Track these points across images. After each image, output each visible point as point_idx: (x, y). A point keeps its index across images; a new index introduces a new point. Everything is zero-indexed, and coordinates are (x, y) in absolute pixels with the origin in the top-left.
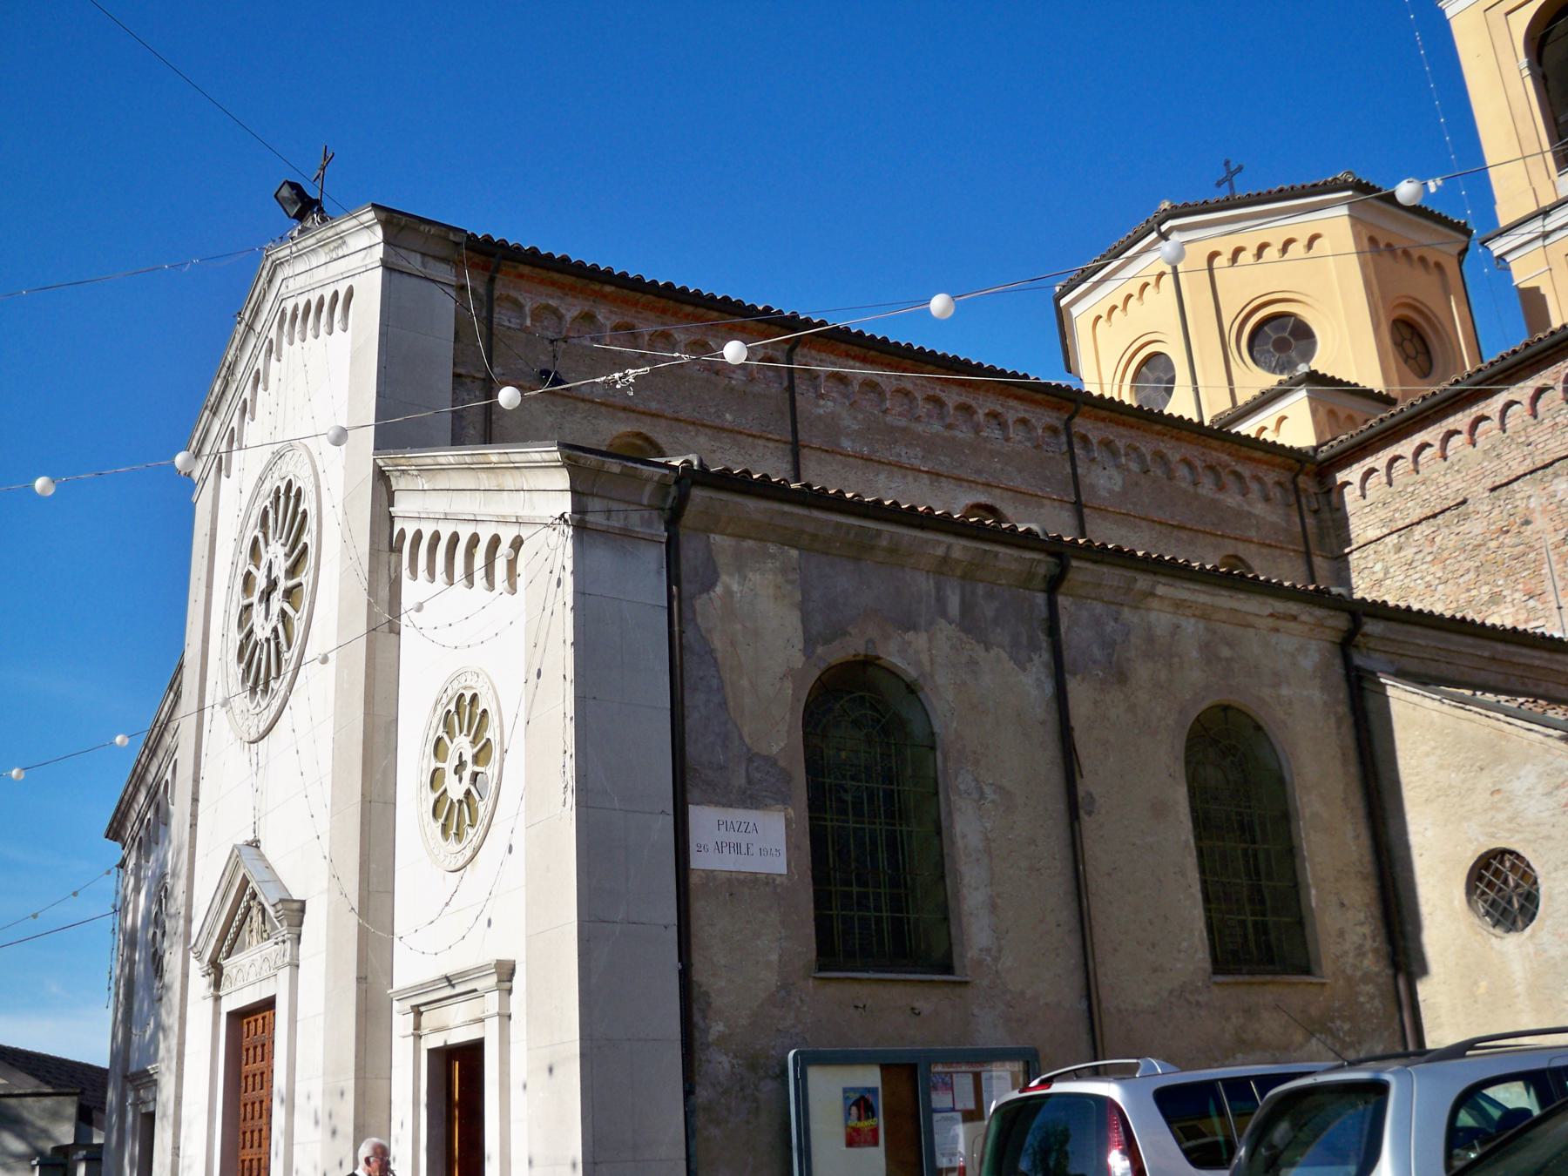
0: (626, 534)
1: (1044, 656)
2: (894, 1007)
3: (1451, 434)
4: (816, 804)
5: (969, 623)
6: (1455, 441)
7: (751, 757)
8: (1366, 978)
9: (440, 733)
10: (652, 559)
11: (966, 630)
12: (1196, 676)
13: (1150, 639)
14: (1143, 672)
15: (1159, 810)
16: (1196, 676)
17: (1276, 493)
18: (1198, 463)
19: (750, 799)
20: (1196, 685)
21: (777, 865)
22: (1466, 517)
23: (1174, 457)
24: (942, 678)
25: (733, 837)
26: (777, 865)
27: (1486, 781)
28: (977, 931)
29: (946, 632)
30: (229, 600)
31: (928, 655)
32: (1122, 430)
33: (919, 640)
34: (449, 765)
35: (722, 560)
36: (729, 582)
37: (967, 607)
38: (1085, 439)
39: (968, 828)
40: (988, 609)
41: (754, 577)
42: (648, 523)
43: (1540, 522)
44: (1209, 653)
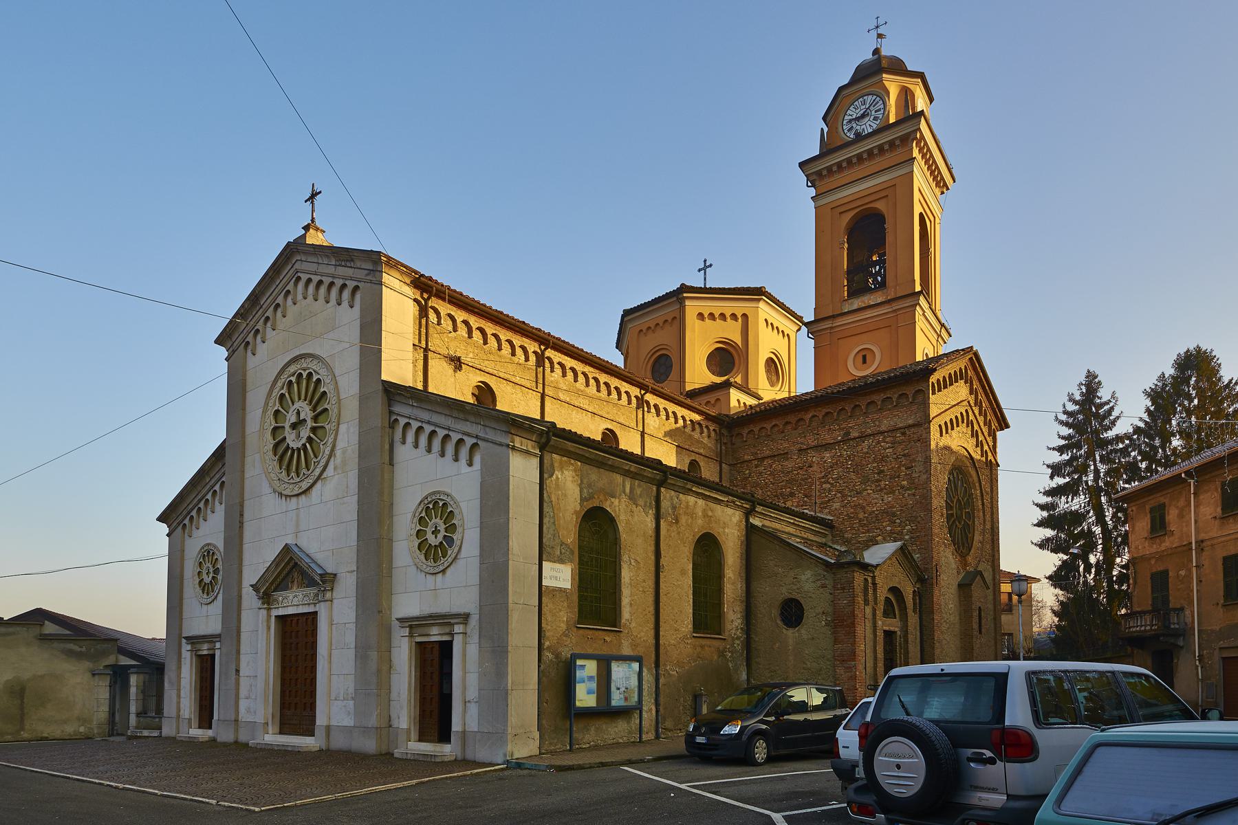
0: (527, 452)
1: (652, 512)
2: (603, 641)
3: (787, 423)
4: (581, 562)
5: (632, 498)
6: (789, 427)
7: (562, 544)
8: (738, 638)
9: (423, 514)
10: (535, 462)
11: (630, 499)
12: (700, 522)
13: (687, 507)
14: (683, 520)
15: (683, 572)
16: (700, 522)
17: (713, 434)
18: (590, 376)
19: (561, 561)
20: (699, 526)
21: (567, 585)
22: (787, 459)
23: (503, 338)
24: (622, 517)
25: (555, 574)
26: (567, 585)
27: (792, 574)
28: (626, 614)
29: (624, 498)
30: (263, 421)
31: (618, 507)
32: (504, 331)
33: (616, 502)
34: (429, 530)
35: (556, 465)
36: (558, 473)
37: (632, 489)
38: (648, 403)
39: (626, 574)
40: (638, 491)
41: (566, 472)
42: (533, 448)
43: (815, 468)
44: (705, 515)
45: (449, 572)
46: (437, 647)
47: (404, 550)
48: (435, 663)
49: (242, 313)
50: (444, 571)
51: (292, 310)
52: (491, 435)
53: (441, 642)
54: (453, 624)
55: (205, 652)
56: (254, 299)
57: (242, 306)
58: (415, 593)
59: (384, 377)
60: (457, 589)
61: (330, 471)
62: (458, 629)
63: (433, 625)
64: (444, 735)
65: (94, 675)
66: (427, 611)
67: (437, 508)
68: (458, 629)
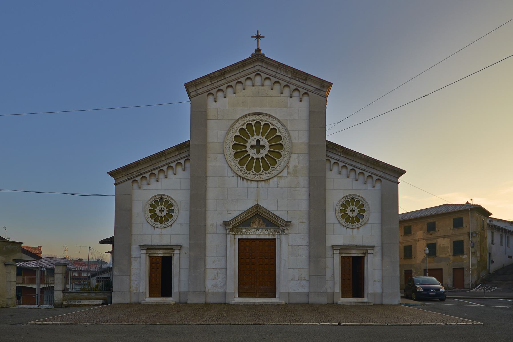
45: (361, 229)
46: (351, 259)
47: (332, 217)
48: (166, 263)
49: (211, 77)
50: (358, 228)
51: (250, 89)
52: (388, 177)
53: (354, 258)
54: (174, 249)
55: (160, 255)
56: (223, 73)
57: (214, 73)
58: (339, 235)
59: (327, 139)
60: (172, 235)
61: (285, 173)
62: (177, 251)
63: (353, 249)
64: (166, 291)
65: (6, 265)
66: (347, 243)
67: (349, 201)
68: (177, 251)
